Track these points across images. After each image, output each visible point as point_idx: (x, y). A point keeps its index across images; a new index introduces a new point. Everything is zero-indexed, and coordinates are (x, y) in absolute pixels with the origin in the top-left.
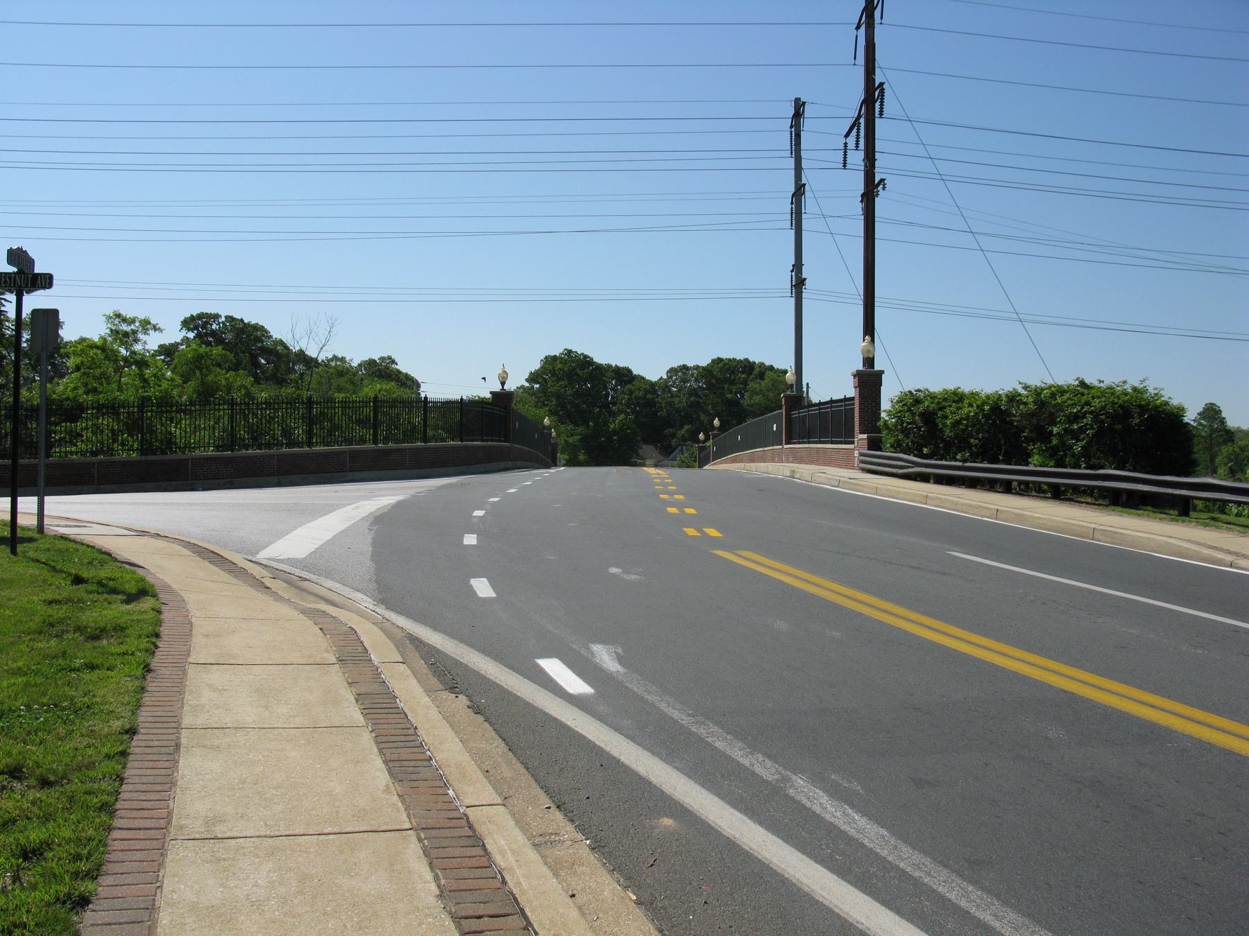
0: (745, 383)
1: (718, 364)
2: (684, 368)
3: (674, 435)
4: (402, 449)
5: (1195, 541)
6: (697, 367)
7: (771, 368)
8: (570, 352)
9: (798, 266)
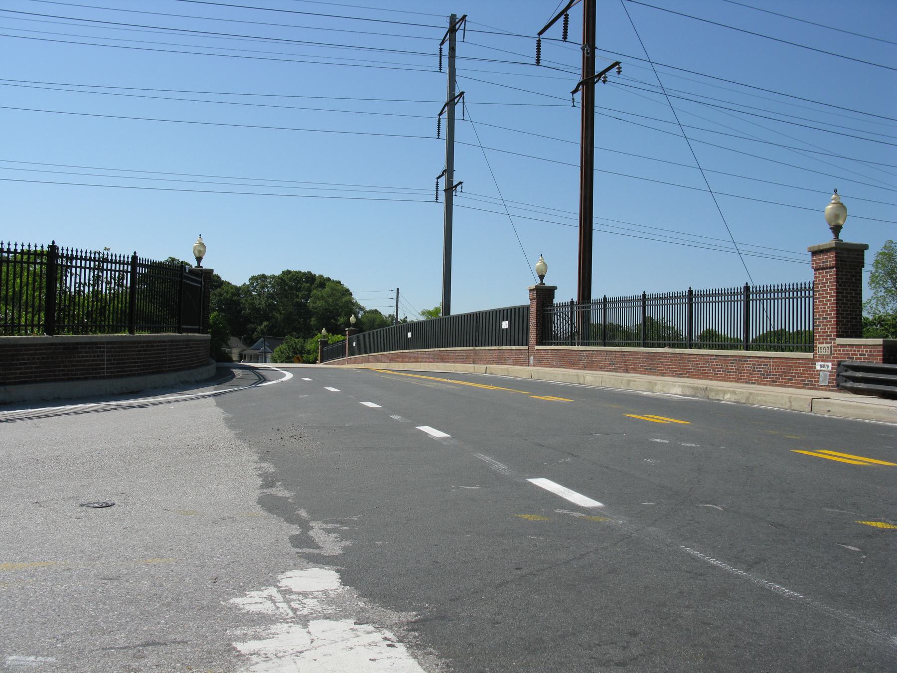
0: (310, 291)
1: (287, 275)
2: (263, 277)
3: (254, 330)
4: (96, 343)
5: (546, 265)
6: (273, 277)
7: (329, 279)
8: (173, 260)
9: (449, 171)
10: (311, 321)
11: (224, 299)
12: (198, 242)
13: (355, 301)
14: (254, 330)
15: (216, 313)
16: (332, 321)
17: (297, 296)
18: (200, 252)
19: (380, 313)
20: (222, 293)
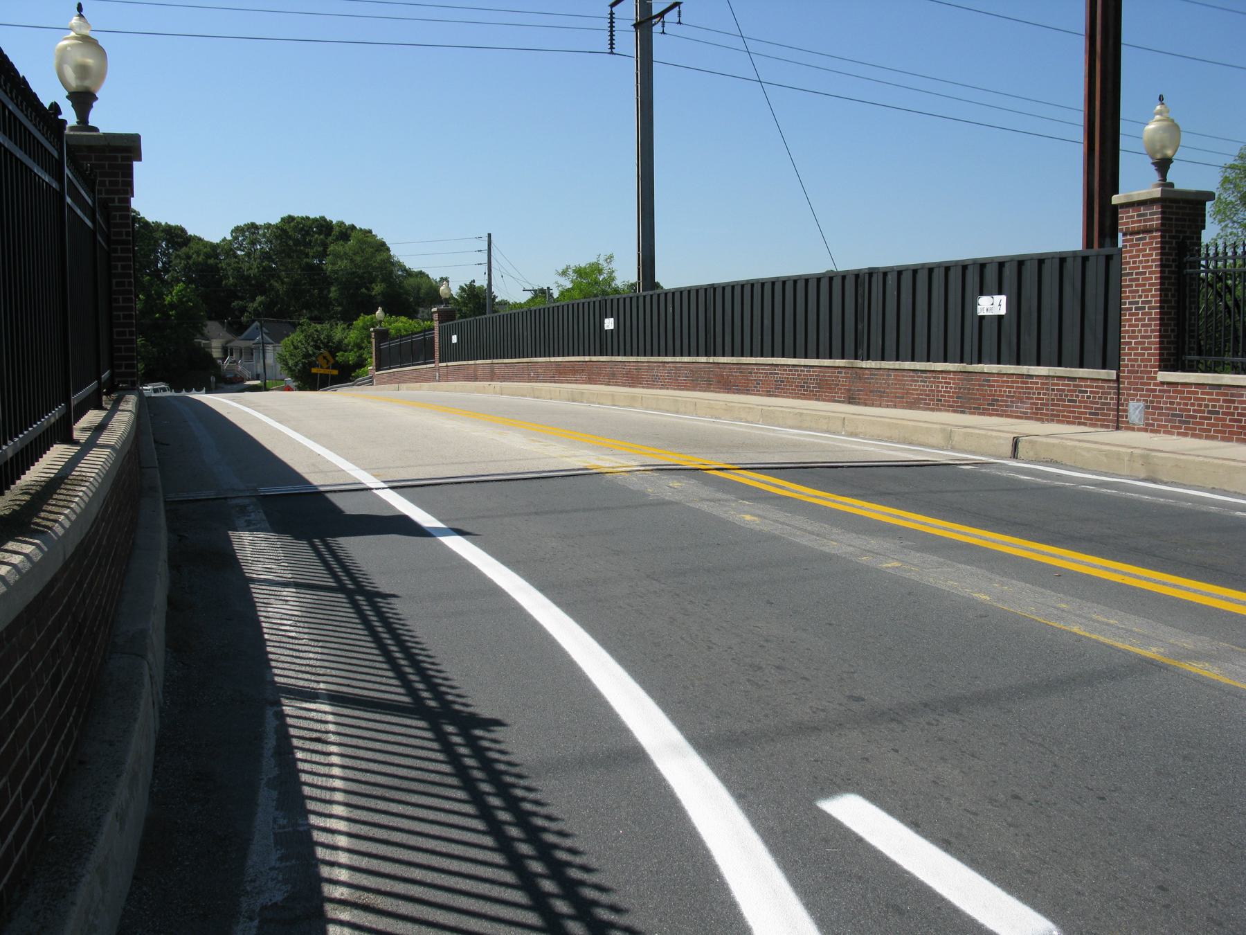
1: (289, 223)
2: (253, 227)
6: (268, 226)
7: (353, 227)
10: (329, 292)
11: (194, 263)
12: (73, 34)
13: (396, 259)
14: (243, 310)
15: (181, 286)
16: (363, 290)
17: (307, 256)
18: (83, 70)
19: (428, 276)
20: (190, 254)
